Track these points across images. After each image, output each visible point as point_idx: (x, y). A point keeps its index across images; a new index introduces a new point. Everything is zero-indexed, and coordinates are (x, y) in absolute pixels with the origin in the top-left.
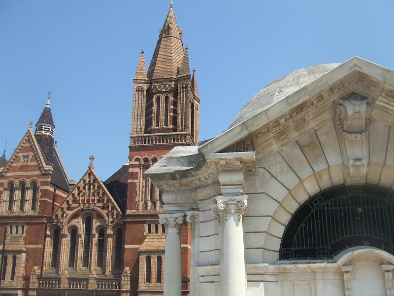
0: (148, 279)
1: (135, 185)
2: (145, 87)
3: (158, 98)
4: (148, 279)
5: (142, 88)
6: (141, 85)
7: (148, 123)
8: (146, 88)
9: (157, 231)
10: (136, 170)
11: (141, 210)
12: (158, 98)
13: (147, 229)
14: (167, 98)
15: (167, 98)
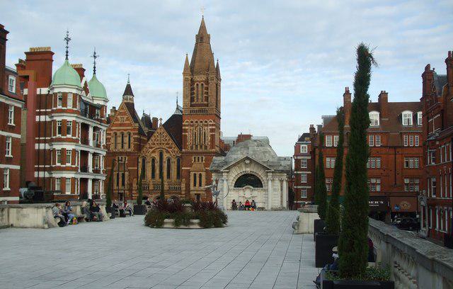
0: (195, 185)
4: (195, 185)
7: (192, 100)
10: (187, 128)
11: (190, 150)
14: (202, 85)
15: (202, 85)
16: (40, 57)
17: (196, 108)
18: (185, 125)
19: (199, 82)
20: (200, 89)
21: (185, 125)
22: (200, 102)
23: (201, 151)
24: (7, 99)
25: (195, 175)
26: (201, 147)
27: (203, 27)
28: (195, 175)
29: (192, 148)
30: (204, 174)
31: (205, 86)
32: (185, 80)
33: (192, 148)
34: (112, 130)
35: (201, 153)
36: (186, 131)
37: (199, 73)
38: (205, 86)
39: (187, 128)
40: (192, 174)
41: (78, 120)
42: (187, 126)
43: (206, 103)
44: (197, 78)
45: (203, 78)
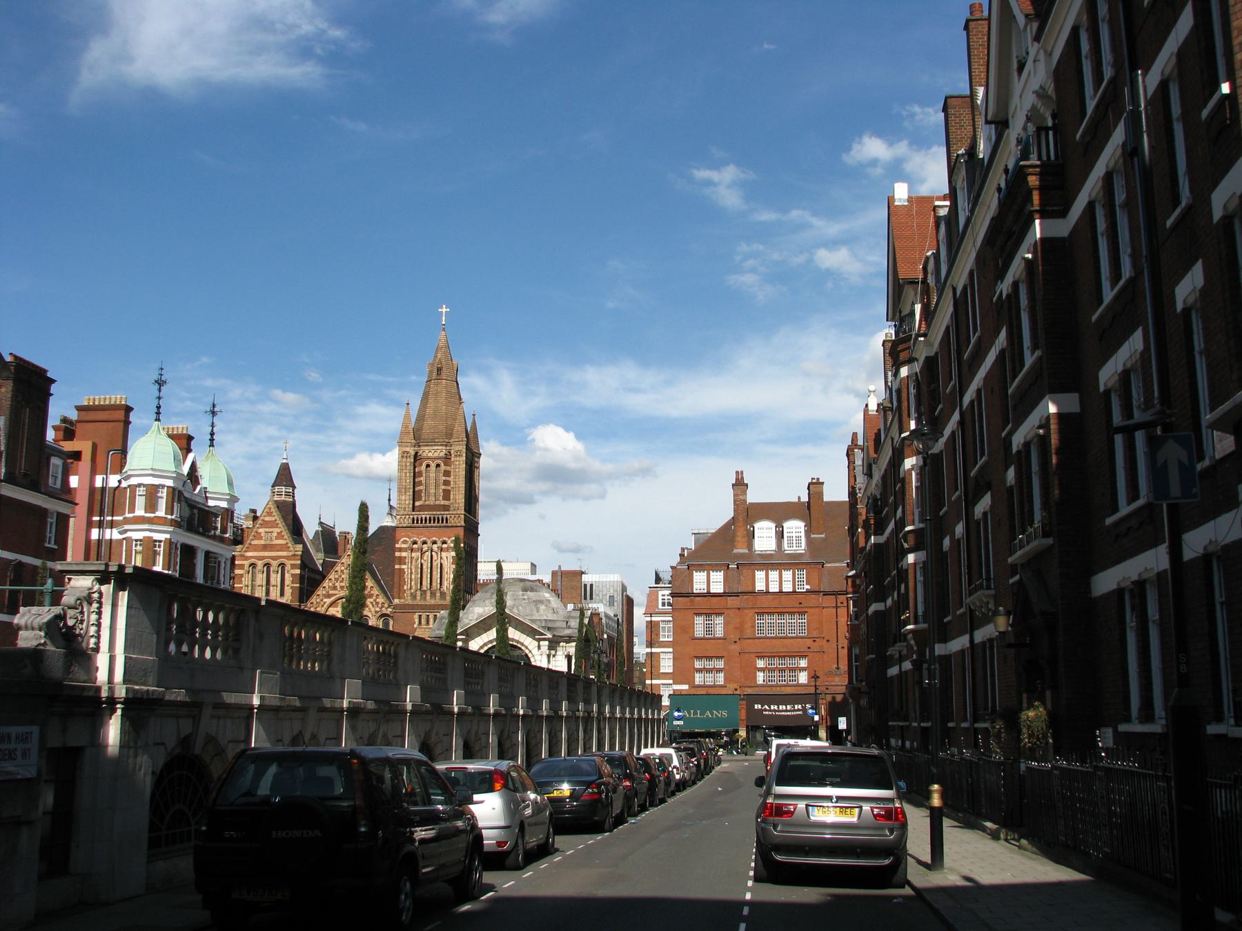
1: (401, 571)
2: (412, 451)
7: (416, 496)
9: (428, 623)
10: (404, 554)
11: (409, 601)
12: (428, 466)
13: (417, 621)
14: (438, 466)
17: (425, 515)
18: (400, 550)
19: (434, 459)
21: (400, 550)
22: (431, 501)
23: (433, 602)
26: (433, 594)
29: (414, 596)
33: (414, 596)
36: (401, 560)
37: (432, 442)
38: (443, 467)
39: (404, 554)
41: (157, 536)
42: (405, 550)
43: (443, 502)
44: (426, 452)
45: (440, 451)
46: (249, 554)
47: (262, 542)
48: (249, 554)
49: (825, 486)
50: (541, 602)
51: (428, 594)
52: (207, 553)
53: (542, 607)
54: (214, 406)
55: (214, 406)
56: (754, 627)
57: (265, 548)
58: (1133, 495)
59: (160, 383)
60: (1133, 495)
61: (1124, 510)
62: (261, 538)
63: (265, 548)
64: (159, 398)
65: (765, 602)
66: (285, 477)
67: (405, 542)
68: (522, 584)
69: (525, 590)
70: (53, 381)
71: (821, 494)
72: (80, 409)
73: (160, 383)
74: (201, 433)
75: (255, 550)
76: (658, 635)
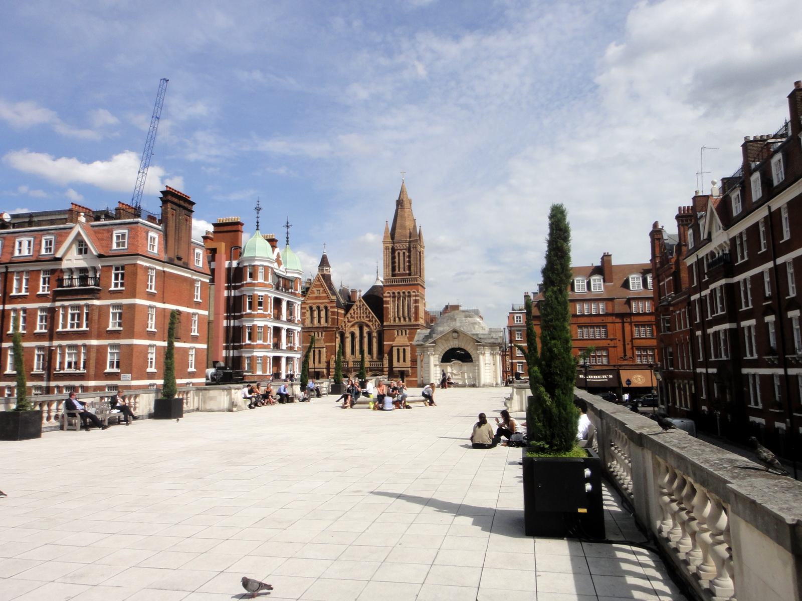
0: (398, 361)
1: (387, 308)
2: (390, 246)
3: (399, 253)
4: (398, 361)
5: (388, 247)
6: (388, 245)
7: (393, 269)
8: (390, 247)
10: (388, 299)
11: (392, 323)
12: (399, 253)
13: (396, 333)
14: (404, 253)
15: (404, 253)
16: (225, 229)
18: (386, 297)
20: (402, 258)
21: (386, 297)
22: (402, 271)
24: (192, 274)
25: (398, 350)
26: (405, 319)
27: (402, 192)
28: (398, 350)
30: (408, 350)
31: (407, 254)
32: (386, 248)
33: (395, 320)
34: (308, 304)
35: (404, 326)
36: (387, 303)
39: (388, 299)
40: (395, 350)
41: (270, 295)
46: (309, 302)
47: (315, 295)
48: (309, 302)
49: (612, 256)
50: (475, 323)
51: (402, 319)
52: (288, 302)
53: (477, 326)
54: (288, 223)
55: (288, 223)
56: (577, 333)
57: (316, 298)
58: (743, 257)
59: (258, 209)
60: (743, 257)
61: (740, 262)
62: (314, 293)
63: (316, 298)
64: (258, 217)
65: (582, 320)
66: (324, 262)
67: (389, 293)
68: (464, 314)
69: (466, 317)
70: (193, 211)
71: (610, 261)
72: (215, 225)
73: (258, 209)
74: (280, 237)
75: (311, 300)
76: (515, 337)
